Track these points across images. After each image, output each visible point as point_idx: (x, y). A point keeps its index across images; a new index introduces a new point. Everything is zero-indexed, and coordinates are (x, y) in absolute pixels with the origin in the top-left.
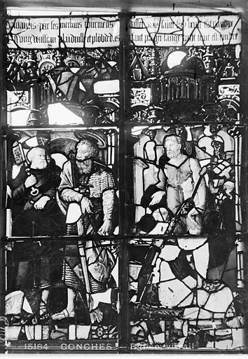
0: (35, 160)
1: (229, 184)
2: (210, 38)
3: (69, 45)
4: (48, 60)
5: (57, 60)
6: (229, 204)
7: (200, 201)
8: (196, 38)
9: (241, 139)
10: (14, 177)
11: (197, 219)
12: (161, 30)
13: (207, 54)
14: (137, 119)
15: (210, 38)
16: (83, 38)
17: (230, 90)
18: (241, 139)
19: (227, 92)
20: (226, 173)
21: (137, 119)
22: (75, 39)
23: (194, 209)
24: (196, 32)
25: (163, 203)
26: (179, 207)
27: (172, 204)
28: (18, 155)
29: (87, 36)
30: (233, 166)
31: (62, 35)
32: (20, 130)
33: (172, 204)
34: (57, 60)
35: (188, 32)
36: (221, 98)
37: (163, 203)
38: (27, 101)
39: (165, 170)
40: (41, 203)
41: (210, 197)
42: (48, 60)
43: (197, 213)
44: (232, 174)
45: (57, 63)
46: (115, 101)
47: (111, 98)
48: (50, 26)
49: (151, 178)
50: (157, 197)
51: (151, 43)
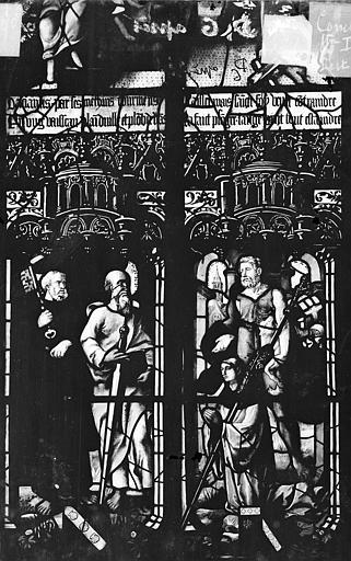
0: (51, 288)
1: (318, 327)
2: (303, 119)
3: (96, 129)
4: (67, 150)
5: (81, 150)
6: (319, 351)
7: (282, 348)
8: (284, 119)
9: (333, 264)
10: (61, 527)
11: (278, 373)
12: (235, 110)
13: (300, 143)
14: (204, 234)
15: (303, 119)
16: (115, 120)
17: (330, 197)
18: (333, 264)
19: (325, 200)
20: (314, 311)
21: (204, 234)
22: (104, 122)
23: (273, 361)
24: (284, 112)
25: (232, 349)
26: (251, 356)
27: (243, 350)
28: (28, 281)
29: (122, 115)
30: (323, 302)
31: (86, 116)
32: (69, 196)
33: (243, 350)
34: (81, 150)
35: (271, 110)
36: (317, 207)
37: (232, 349)
38: (39, 206)
39: (238, 303)
40: (61, 349)
41: (294, 341)
42: (67, 150)
43: (276, 364)
44: (321, 313)
45: (80, 153)
46: (159, 212)
47: (154, 207)
48: (69, 104)
49: (217, 313)
50: (224, 342)
51: (220, 128)
